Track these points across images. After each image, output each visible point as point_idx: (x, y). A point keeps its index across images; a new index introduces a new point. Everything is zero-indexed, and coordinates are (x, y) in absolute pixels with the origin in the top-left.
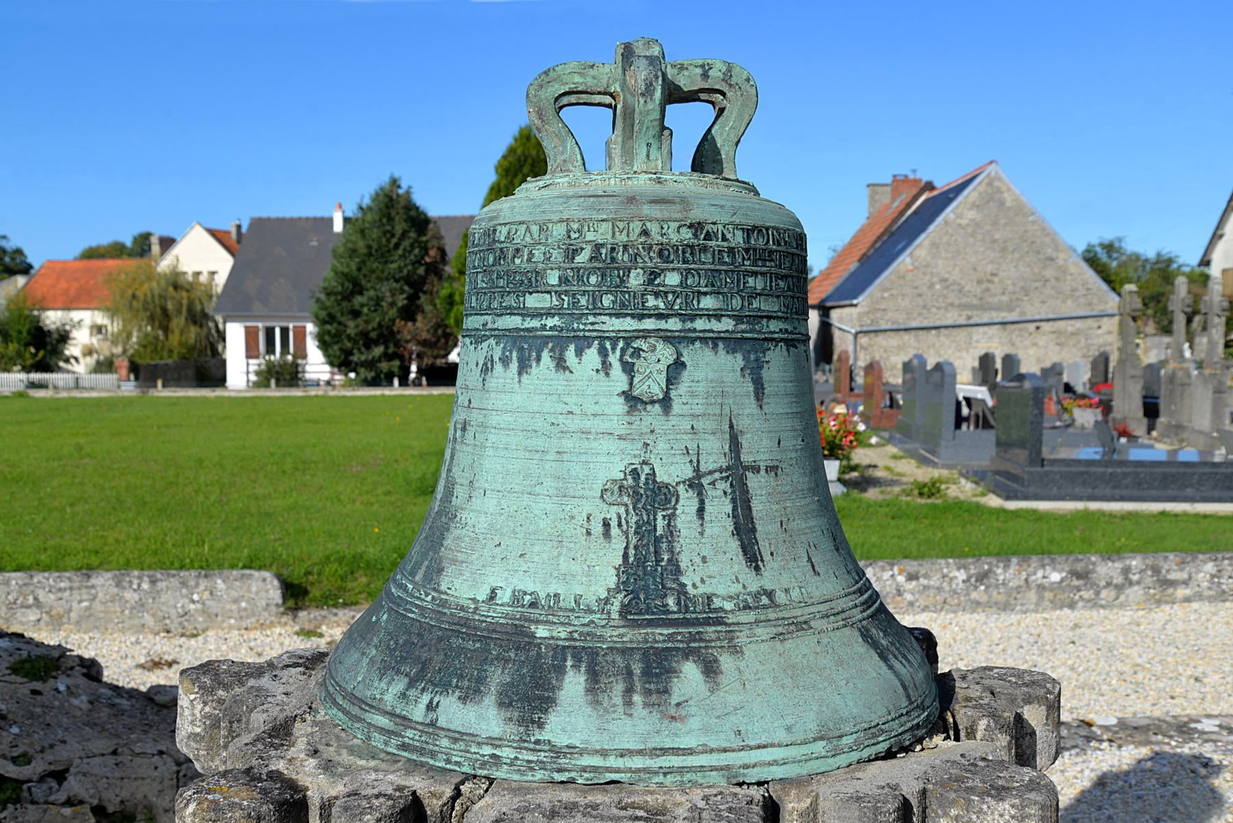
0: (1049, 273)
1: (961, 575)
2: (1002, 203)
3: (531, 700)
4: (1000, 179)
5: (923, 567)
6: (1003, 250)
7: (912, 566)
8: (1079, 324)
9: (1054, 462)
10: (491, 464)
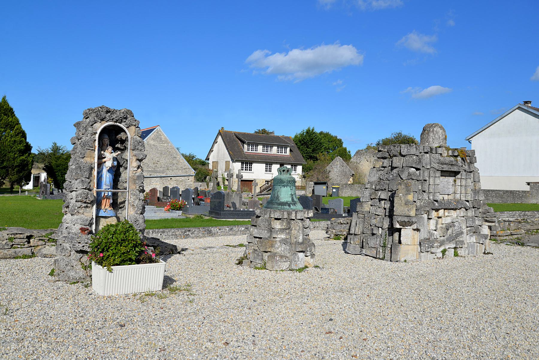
0: (174, 162)
1: (228, 229)
2: (161, 139)
3: (289, 206)
4: (161, 131)
5: (221, 228)
6: (161, 154)
7: (220, 227)
8: (183, 178)
9: (226, 211)
10: (282, 193)
